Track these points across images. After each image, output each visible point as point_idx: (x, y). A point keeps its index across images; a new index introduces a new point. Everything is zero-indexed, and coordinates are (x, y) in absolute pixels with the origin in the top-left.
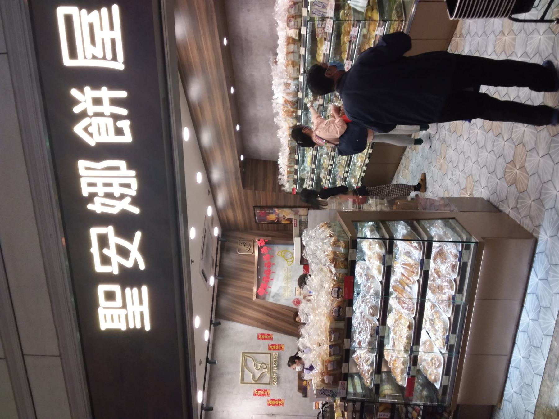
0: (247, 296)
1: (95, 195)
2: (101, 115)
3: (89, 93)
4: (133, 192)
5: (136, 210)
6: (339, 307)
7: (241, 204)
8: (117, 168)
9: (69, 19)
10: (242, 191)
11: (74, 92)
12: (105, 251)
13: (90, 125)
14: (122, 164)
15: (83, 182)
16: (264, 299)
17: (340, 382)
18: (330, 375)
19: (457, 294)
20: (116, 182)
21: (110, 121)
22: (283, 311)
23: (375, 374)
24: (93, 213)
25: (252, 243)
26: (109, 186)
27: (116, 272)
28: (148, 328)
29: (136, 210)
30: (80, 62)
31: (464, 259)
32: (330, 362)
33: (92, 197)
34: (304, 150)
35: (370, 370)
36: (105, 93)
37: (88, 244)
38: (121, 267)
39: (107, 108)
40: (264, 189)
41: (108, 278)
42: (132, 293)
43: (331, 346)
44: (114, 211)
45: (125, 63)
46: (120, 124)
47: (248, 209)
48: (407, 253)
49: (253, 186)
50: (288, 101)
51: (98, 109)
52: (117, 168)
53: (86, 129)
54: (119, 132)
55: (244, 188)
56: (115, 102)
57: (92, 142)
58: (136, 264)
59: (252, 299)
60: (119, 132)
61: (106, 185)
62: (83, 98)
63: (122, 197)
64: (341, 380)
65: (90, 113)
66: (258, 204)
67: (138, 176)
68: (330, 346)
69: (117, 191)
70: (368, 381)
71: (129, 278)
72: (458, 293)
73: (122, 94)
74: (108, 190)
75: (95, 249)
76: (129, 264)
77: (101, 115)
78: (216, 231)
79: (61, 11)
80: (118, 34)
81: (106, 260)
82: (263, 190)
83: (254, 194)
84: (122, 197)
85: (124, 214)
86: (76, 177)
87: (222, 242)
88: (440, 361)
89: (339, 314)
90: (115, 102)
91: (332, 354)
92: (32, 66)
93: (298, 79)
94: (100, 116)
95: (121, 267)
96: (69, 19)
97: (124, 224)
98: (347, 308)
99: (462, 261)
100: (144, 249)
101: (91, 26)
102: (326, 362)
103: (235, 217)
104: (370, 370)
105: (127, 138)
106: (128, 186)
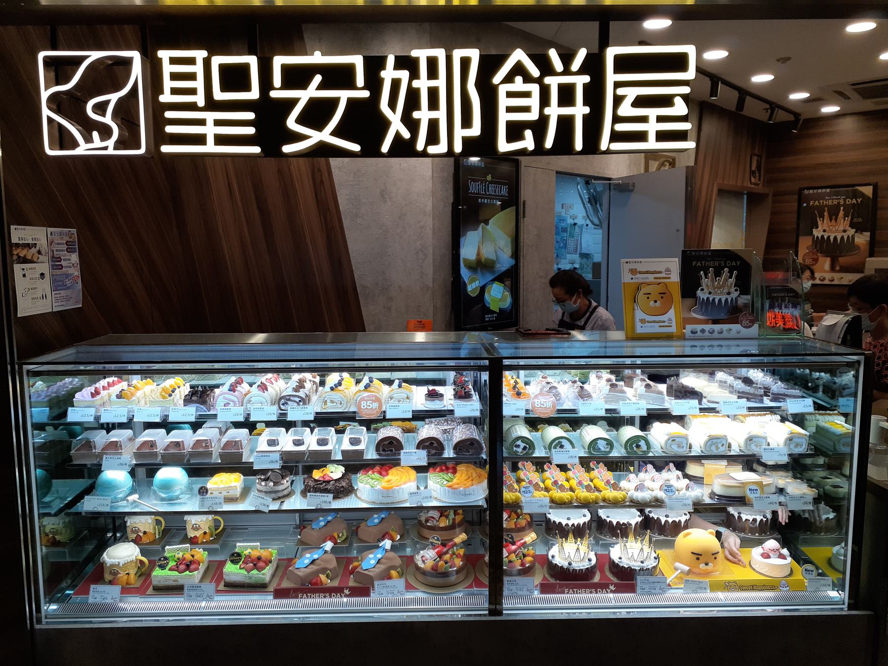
1: (414, 75)
2: (545, 101)
8: (467, 122)
16: (500, 613)
21: (534, 116)
34: (17, 245)
36: (579, 110)
39: (554, 111)
46: (528, 134)
52: (467, 122)
54: (515, 131)
60: (515, 131)
61: (433, 93)
63: (412, 125)
69: (423, 115)
81: (297, 77)
84: (412, 125)
101: (667, 101)
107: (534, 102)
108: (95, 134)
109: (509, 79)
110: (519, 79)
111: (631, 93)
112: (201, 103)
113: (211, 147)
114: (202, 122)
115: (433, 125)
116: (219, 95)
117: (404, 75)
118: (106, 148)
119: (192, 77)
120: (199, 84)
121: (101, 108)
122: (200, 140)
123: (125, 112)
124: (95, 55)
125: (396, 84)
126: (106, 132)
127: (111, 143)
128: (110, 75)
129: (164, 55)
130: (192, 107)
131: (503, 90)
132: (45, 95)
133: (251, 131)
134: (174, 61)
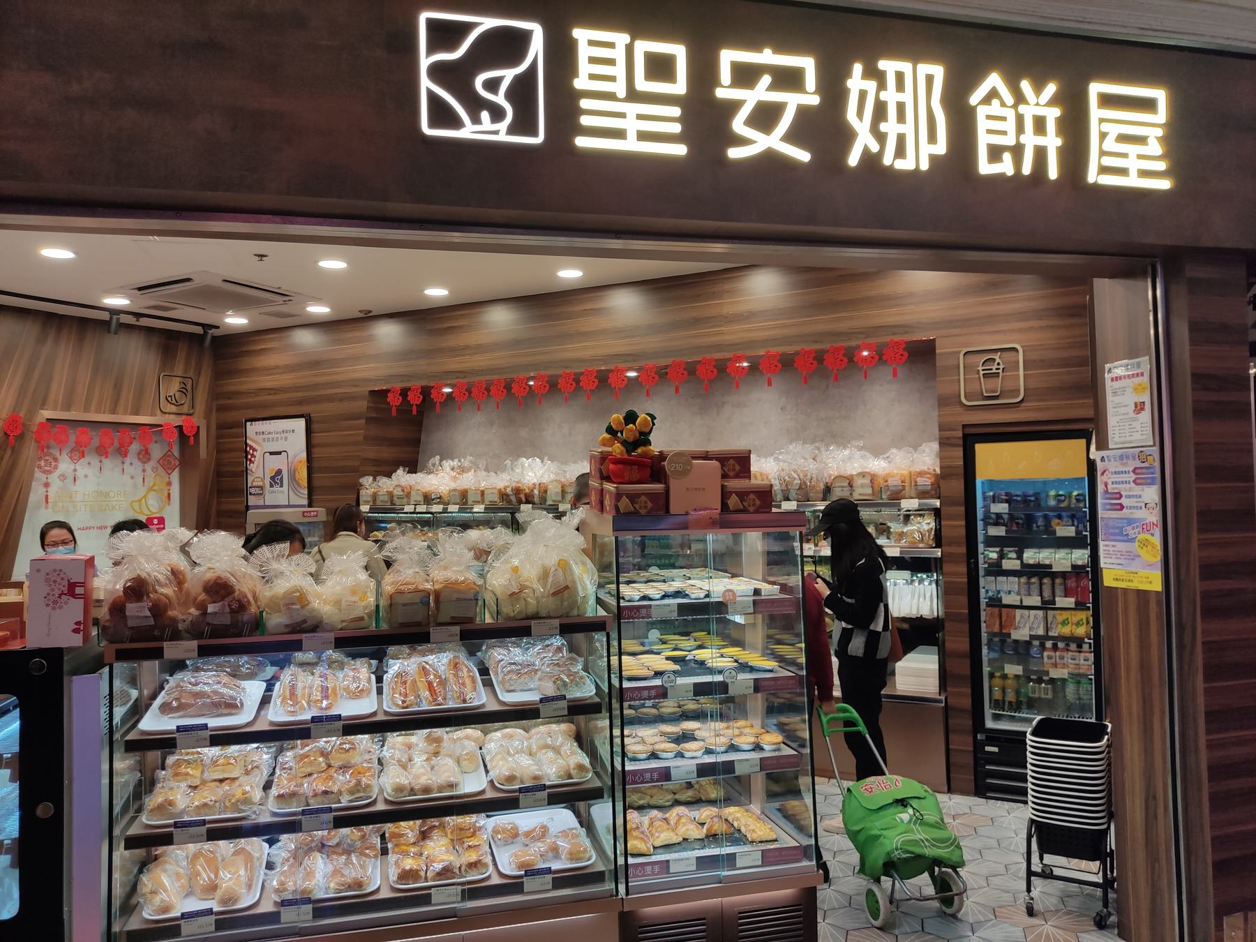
0: (52, 396)
1: (882, 86)
2: (1020, 129)
3: (1053, 114)
4: (887, 160)
5: (853, 159)
7: (316, 386)
8: (932, 138)
11: (1051, 89)
12: (766, 80)
14: (941, 148)
15: (905, 67)
19: (213, 918)
20: (908, 129)
21: (1010, 141)
22: (11, 493)
24: (847, 73)
25: (185, 409)
26: (899, 113)
28: (581, 142)
29: (853, 159)
30: (1096, 112)
31: (529, 884)
36: (1053, 142)
41: (703, 74)
42: (669, 119)
46: (1007, 157)
48: (179, 793)
50: (546, 492)
51: (1029, 125)
52: (932, 138)
54: (995, 153)
55: (372, 393)
56: (1040, 153)
57: (974, 99)
58: (742, 141)
60: (995, 153)
61: (901, 107)
62: (1042, 101)
63: (881, 138)
65: (1022, 109)
66: (315, 427)
67: (916, 172)
69: (890, 127)
71: (706, 118)
73: (1053, 173)
74: (892, 112)
75: (767, 57)
76: (738, 124)
77: (1020, 129)
78: (236, 321)
80: (1132, 181)
81: (745, 76)
82: (365, 437)
84: (881, 138)
85: (846, 136)
86: (916, 57)
87: (202, 338)
90: (1040, 153)
93: (787, 499)
95: (734, 106)
96: (1148, 105)
97: (823, 127)
100: (770, 159)
101: (1141, 140)
103: (269, 370)
105: (985, 168)
106: (900, 152)
107: (1010, 125)
108: (485, 115)
109: (987, 100)
110: (995, 102)
111: (1114, 130)
112: (622, 93)
113: (631, 145)
114: (622, 115)
115: (901, 139)
116: (642, 84)
117: (871, 86)
118: (496, 132)
119: (611, 62)
120: (620, 71)
121: (492, 85)
122: (620, 134)
123: (522, 91)
124: (488, 23)
125: (863, 95)
126: (497, 114)
127: (503, 126)
128: (506, 47)
129: (581, 35)
130: (611, 96)
131: (982, 112)
132: (425, 62)
133: (676, 128)
134: (592, 43)
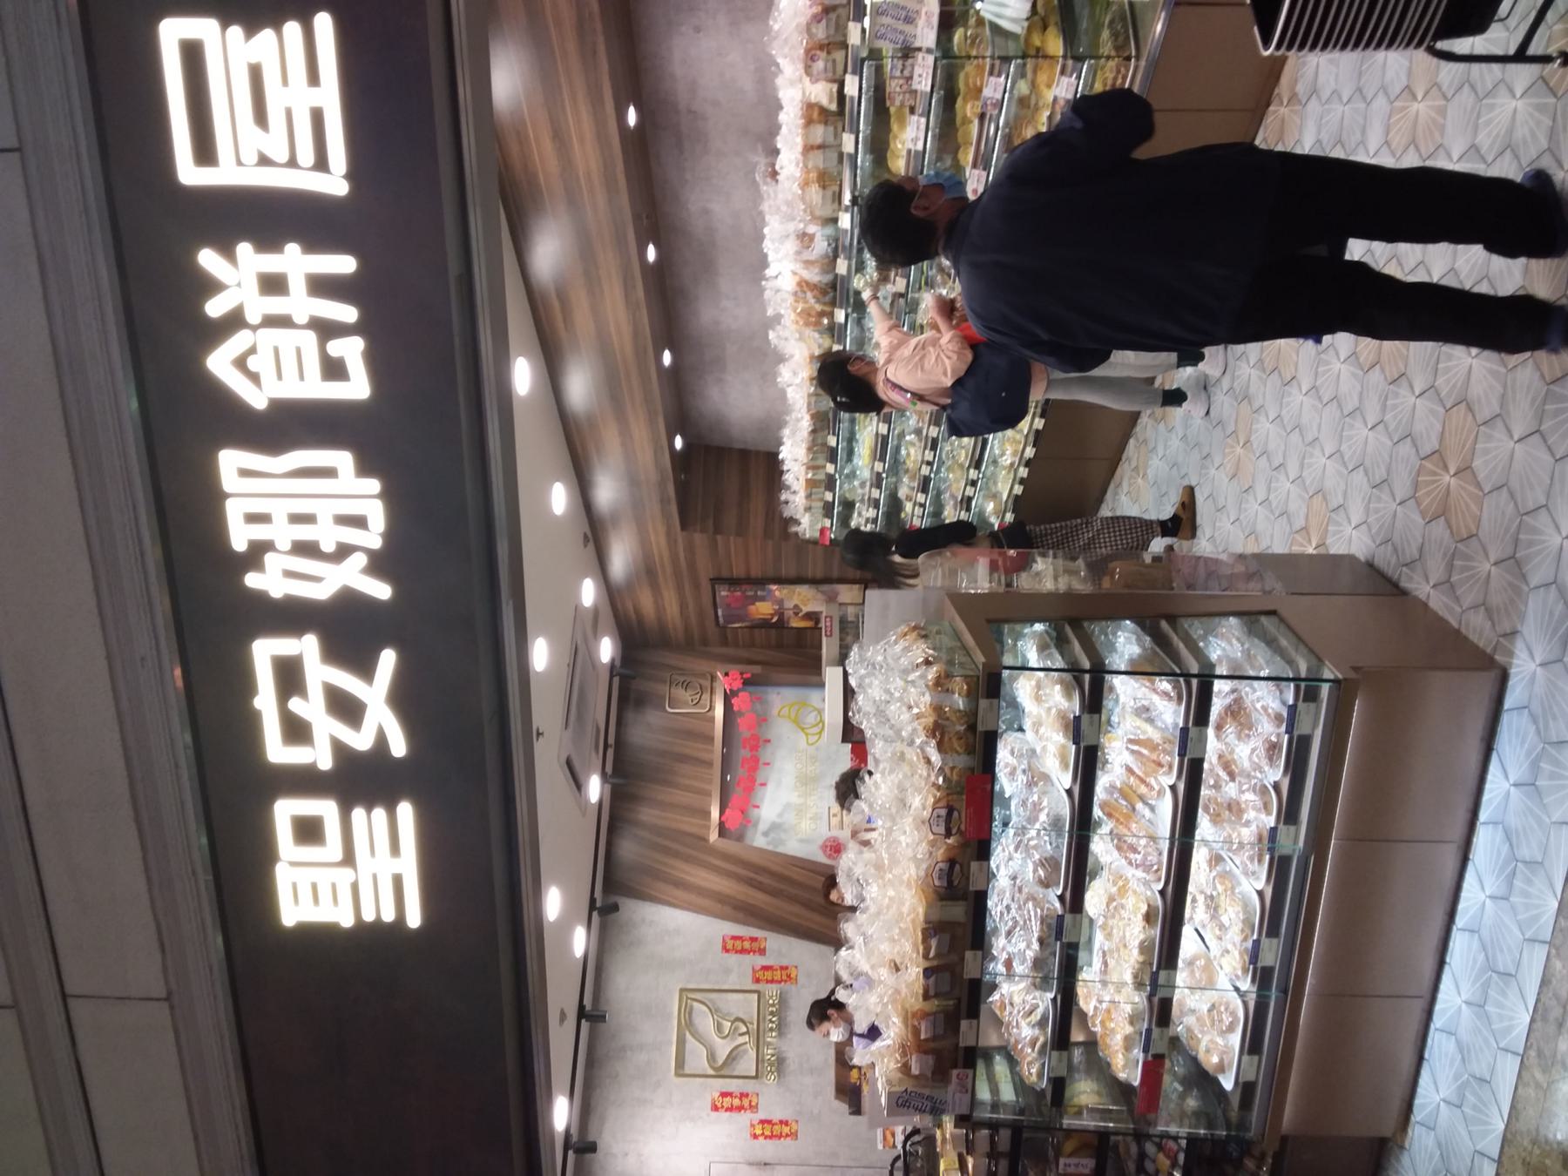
0: (694, 830)
1: (267, 546)
2: (283, 322)
3: (250, 260)
4: (373, 539)
5: (381, 590)
6: (952, 862)
7: (677, 573)
8: (329, 473)
9: (192, 54)
10: (680, 536)
11: (208, 259)
12: (295, 704)
13: (252, 350)
14: (342, 459)
15: (234, 511)
17: (955, 1072)
18: (926, 1052)
19: (1281, 826)
20: (326, 511)
21: (309, 339)
22: (795, 874)
23: (1053, 1048)
24: (260, 598)
25: (707, 683)
26: (305, 522)
27: (325, 763)
28: (414, 920)
29: (381, 590)
30: (225, 174)
31: (1302, 728)
32: (925, 1015)
33: (258, 552)
35: (1037, 1039)
36: (295, 261)
37: (247, 686)
38: (339, 749)
39: (301, 304)
40: (742, 529)
41: (304, 781)
42: (369, 822)
43: (927, 972)
44: (321, 592)
45: (351, 176)
46: (336, 347)
47: (696, 586)
48: (1142, 709)
49: (711, 522)
50: (807, 283)
51: (275, 305)
52: (329, 473)
53: (241, 363)
54: (334, 369)
55: (684, 526)
56: (322, 286)
57: (257, 400)
58: (381, 740)
59: (706, 840)
60: (334, 369)
61: (296, 519)
62: (234, 275)
63: (343, 552)
64: (955, 1067)
65: (253, 317)
66: (725, 574)
67: (387, 495)
68: (926, 971)
69: (328, 536)
70: (1034, 1071)
71: (361, 780)
72: (1286, 823)
73: (343, 264)
74: (304, 533)
75: (265, 700)
76: (361, 741)
77: (283, 322)
78: (606, 650)
79: (172, 32)
80: (330, 96)
81: (296, 731)
82: (738, 534)
83: (714, 546)
84: (343, 552)
85: (349, 601)
86: (214, 498)
87: (623, 678)
88: (1233, 1014)
89: (950, 882)
90: (322, 286)
91: (932, 993)
92: (89, 184)
93: (835, 220)
94: (280, 327)
95: (339, 749)
96: (192, 54)
97: (347, 630)
98: (974, 865)
99: (1296, 733)
100: (403, 699)
101: (256, 73)
102: (914, 1015)
103: (659, 608)
104: (1037, 1039)
105: (357, 387)
106: (359, 522)
